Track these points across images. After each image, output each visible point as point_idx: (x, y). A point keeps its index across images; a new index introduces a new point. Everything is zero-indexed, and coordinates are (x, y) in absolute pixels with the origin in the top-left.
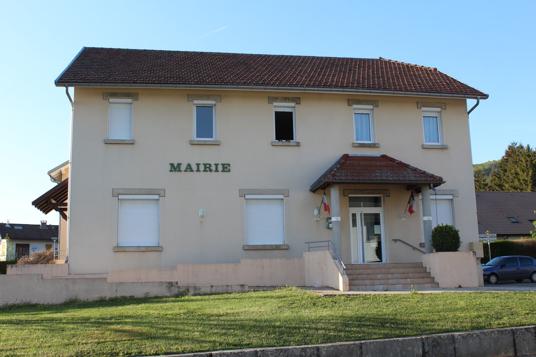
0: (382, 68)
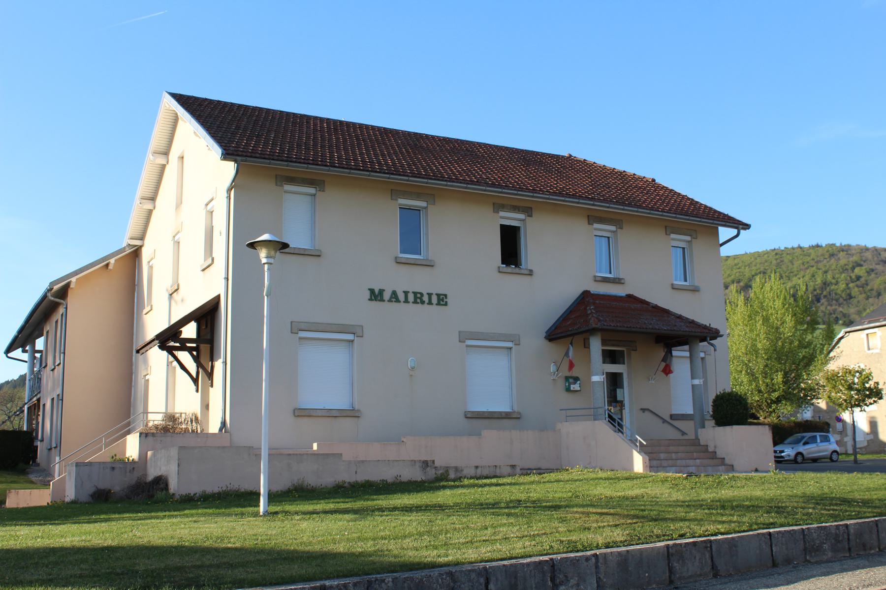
0: (322, 131)
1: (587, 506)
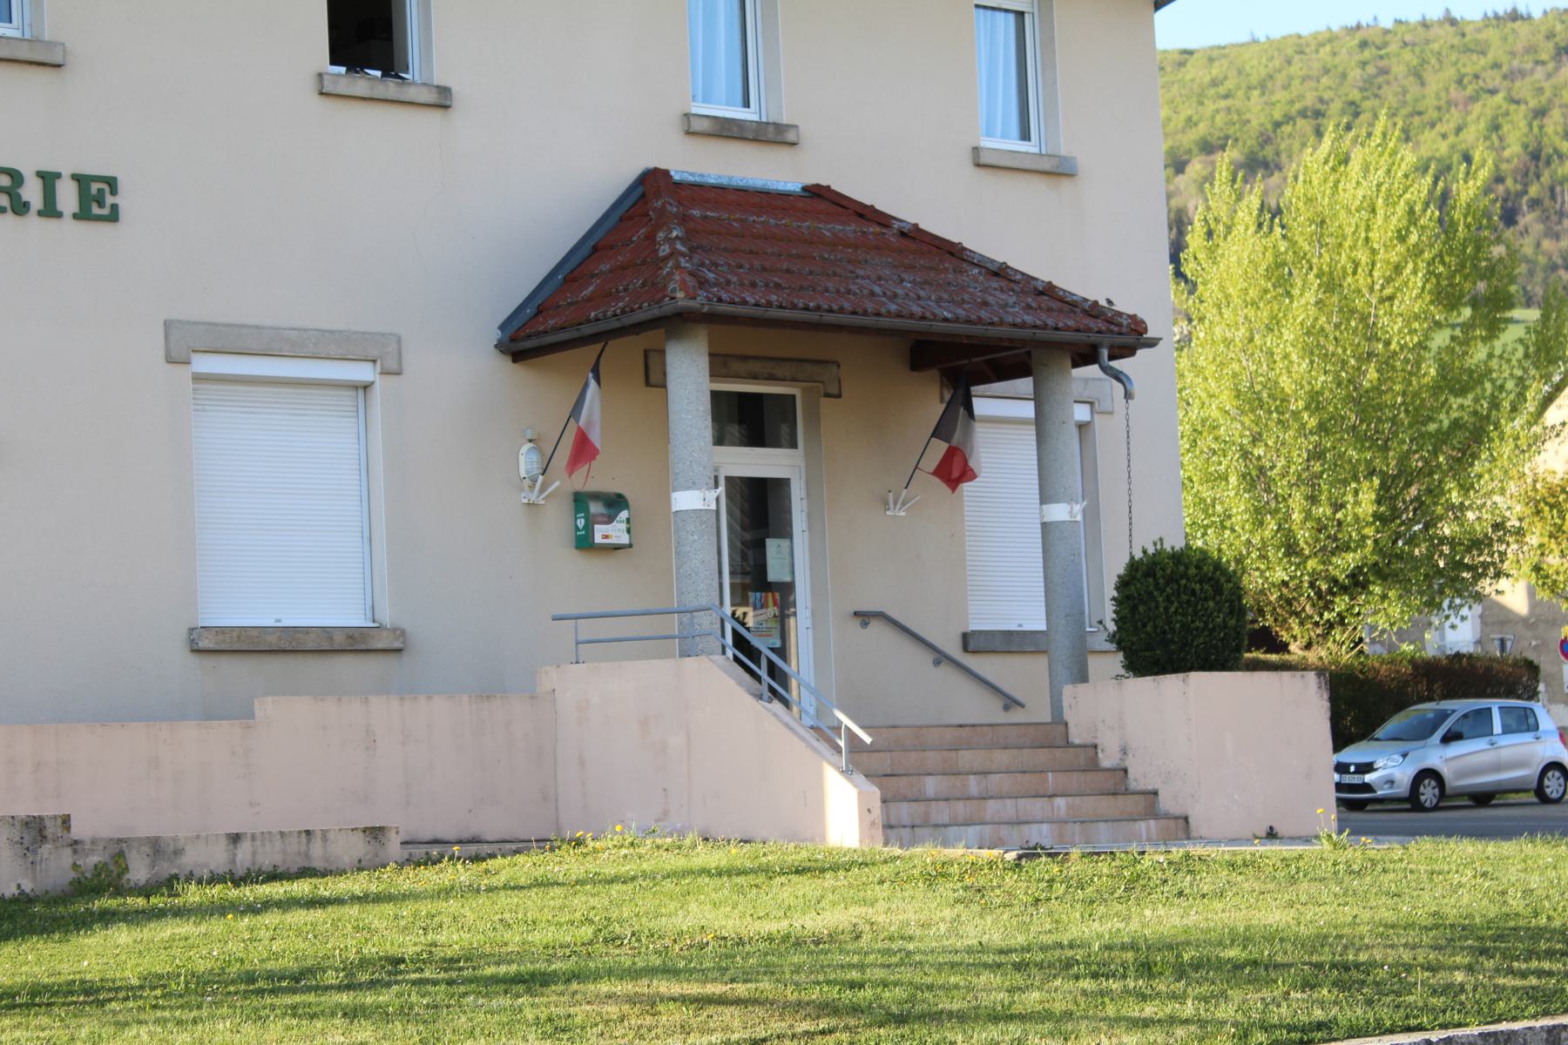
1: (651, 972)
